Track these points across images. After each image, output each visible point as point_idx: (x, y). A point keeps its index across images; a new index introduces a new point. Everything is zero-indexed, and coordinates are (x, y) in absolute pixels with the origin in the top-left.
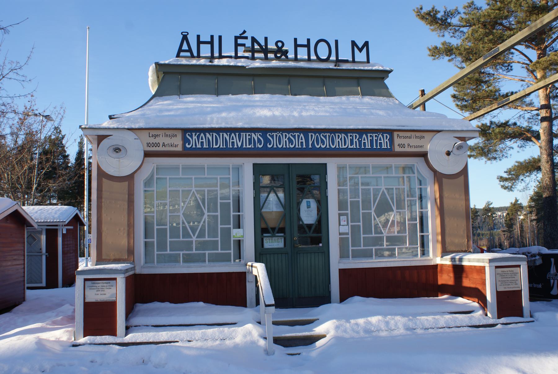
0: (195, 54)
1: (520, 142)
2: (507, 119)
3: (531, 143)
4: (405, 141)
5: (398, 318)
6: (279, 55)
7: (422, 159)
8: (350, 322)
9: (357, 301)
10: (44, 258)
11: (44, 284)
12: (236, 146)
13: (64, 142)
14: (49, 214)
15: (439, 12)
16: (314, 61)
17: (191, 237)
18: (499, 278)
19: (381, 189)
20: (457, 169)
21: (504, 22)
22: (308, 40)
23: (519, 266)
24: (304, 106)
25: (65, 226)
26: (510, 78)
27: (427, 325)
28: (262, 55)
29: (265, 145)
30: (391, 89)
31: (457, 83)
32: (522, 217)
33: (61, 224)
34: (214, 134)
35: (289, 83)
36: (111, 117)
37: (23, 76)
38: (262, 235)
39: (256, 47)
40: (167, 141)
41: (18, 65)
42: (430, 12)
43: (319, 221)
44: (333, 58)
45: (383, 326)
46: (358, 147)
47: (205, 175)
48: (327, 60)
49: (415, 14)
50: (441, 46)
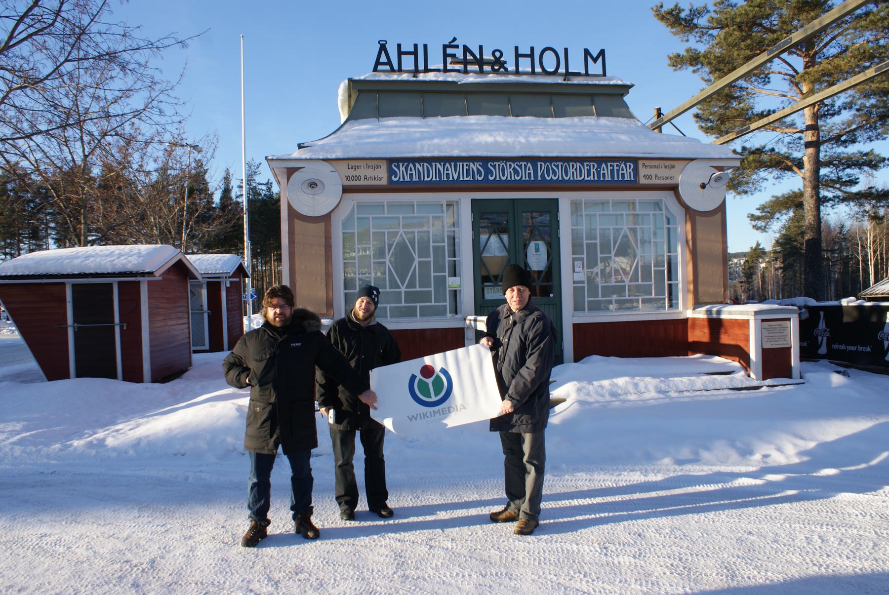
0: (396, 67)
1: (776, 173)
2: (763, 144)
3: (790, 173)
4: (652, 172)
5: (648, 379)
6: (496, 68)
7: (672, 193)
8: (593, 384)
9: (596, 362)
10: (206, 316)
11: (207, 347)
12: (451, 179)
13: (207, 176)
14: (209, 264)
15: (683, 10)
16: (539, 74)
17: (399, 287)
18: (765, 333)
19: (622, 229)
20: (716, 204)
21: (763, 22)
22: (532, 49)
23: (789, 319)
24: (531, 129)
25: (229, 277)
26: (768, 92)
27: (682, 388)
28: (476, 68)
29: (486, 177)
30: (633, 109)
31: (705, 101)
32: (763, 265)
33: (224, 275)
34: (426, 164)
35: (509, 102)
36: (300, 146)
37: (175, 98)
38: (483, 283)
39: (468, 58)
40: (370, 173)
41: (170, 85)
42: (673, 10)
43: (550, 267)
44: (562, 70)
45: (631, 388)
46: (596, 179)
47: (414, 213)
48: (555, 73)
49: (653, 13)
50: (685, 54)
